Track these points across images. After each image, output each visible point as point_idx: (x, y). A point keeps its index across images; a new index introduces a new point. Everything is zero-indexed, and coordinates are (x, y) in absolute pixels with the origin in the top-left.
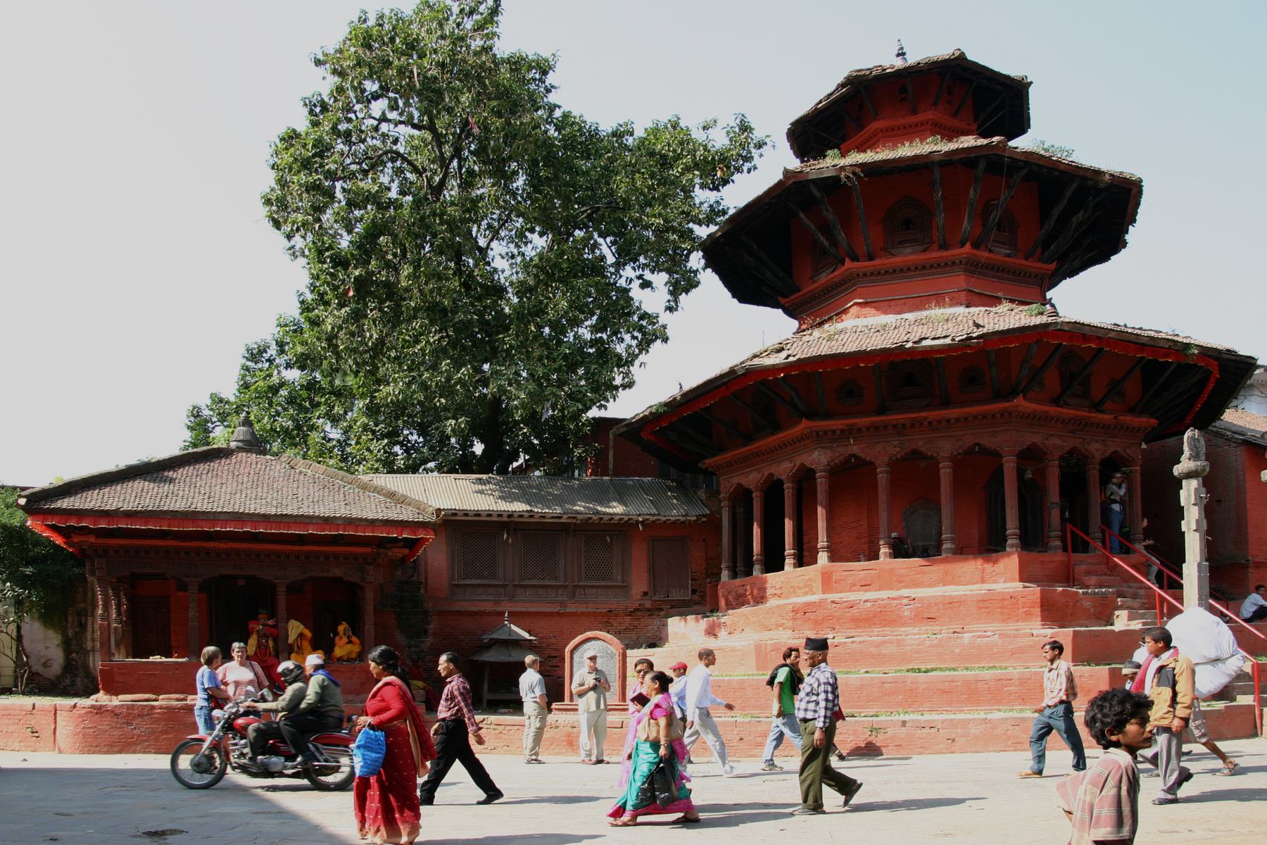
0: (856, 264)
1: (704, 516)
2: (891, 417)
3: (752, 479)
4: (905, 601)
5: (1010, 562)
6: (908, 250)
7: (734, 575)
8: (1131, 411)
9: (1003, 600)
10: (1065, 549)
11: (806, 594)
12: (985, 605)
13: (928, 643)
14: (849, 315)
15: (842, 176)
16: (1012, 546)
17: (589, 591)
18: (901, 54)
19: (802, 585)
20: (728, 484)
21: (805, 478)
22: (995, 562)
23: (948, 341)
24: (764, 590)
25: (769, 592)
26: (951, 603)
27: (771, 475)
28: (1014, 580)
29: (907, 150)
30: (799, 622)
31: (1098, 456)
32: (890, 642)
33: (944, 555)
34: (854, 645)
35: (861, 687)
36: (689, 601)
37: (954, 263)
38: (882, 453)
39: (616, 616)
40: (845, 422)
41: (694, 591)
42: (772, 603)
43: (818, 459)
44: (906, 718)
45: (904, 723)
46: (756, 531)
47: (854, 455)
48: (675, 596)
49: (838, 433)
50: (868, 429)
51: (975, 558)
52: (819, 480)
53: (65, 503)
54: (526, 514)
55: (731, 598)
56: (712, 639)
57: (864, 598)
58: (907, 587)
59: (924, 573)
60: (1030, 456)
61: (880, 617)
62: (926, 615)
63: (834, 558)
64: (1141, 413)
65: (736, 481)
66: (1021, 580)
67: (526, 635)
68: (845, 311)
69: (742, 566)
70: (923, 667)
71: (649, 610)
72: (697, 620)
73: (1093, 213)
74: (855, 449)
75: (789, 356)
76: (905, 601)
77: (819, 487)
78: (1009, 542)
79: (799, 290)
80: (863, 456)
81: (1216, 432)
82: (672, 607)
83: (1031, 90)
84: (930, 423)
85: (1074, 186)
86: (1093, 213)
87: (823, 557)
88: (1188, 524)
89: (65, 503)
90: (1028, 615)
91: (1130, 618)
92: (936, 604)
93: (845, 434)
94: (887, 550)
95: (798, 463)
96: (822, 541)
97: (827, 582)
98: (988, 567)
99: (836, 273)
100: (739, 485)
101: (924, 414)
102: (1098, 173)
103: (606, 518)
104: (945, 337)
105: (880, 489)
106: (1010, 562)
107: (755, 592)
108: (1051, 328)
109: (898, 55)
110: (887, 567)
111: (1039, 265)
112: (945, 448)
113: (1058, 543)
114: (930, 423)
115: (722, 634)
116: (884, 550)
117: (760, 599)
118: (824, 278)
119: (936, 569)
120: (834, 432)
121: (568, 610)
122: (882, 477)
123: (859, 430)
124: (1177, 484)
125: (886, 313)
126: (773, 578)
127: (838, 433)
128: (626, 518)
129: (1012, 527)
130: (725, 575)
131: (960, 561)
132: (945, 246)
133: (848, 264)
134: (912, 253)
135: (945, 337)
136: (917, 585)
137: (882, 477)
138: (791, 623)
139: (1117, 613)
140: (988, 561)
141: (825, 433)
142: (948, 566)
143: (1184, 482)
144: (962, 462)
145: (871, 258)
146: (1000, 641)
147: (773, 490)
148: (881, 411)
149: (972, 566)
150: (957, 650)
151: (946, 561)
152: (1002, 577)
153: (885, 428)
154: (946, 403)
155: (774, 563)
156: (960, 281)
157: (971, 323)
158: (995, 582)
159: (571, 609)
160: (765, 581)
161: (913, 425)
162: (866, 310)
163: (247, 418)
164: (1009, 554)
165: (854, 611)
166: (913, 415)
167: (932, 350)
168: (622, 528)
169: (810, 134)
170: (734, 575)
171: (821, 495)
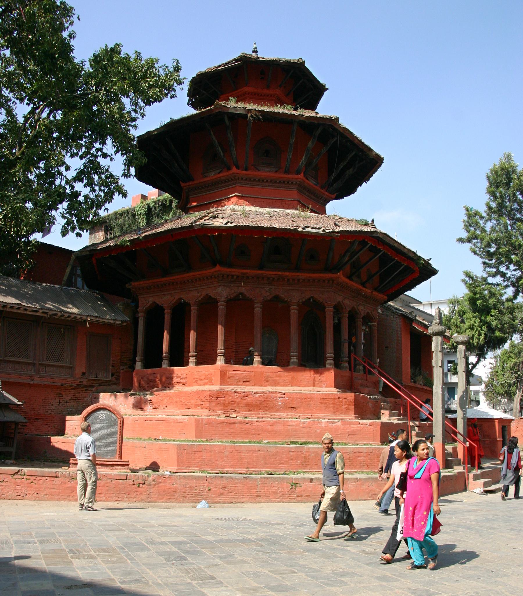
0: (238, 171)
1: (125, 321)
2: (267, 272)
3: (166, 300)
4: (279, 395)
5: (330, 375)
6: (267, 169)
7: (146, 365)
9: (335, 399)
10: (350, 370)
11: (205, 384)
12: (325, 401)
13: (302, 425)
14: (230, 202)
15: (249, 114)
16: (330, 364)
17: (48, 369)
18: (255, 51)
19: (202, 378)
20: (146, 301)
21: (208, 306)
22: (321, 373)
23: (320, 231)
24: (171, 378)
25: (175, 380)
26: (305, 399)
27: (181, 299)
28: (330, 387)
29: (278, 109)
30: (214, 404)
31: (363, 314)
32: (279, 423)
33: (291, 366)
34: (258, 423)
35: (276, 454)
36: (110, 381)
38: (258, 294)
39: (66, 389)
40: (241, 271)
41: (113, 375)
42: (177, 389)
43: (222, 293)
44: (313, 476)
45: (311, 480)
46: (166, 336)
47: (242, 294)
48: (102, 377)
49: (235, 277)
50: (253, 277)
51: (310, 370)
54: (16, 306)
55: (143, 382)
56: (139, 412)
57: (255, 391)
58: (270, 385)
59: (281, 376)
60: (338, 309)
61: (263, 405)
62: (291, 406)
63: (227, 362)
65: (151, 300)
66: (335, 387)
67: (15, 401)
68: (229, 199)
69: (153, 360)
70: (300, 441)
71: (85, 386)
72: (126, 397)
74: (243, 290)
75: (228, 222)
76: (279, 395)
79: (193, 180)
80: (248, 295)
81: (387, 307)
82: (100, 385)
83: (326, 93)
84: (288, 280)
85: (353, 154)
86: (350, 164)
87: (220, 361)
88: (437, 362)
90: (348, 409)
91: (390, 416)
92: (297, 399)
94: (259, 359)
95: (204, 294)
96: (220, 349)
97: (224, 378)
98: (317, 376)
99: (221, 175)
100: (154, 302)
101: (287, 273)
102: (370, 150)
103: (66, 315)
104: (319, 228)
105: (292, 322)
106: (330, 375)
107: (164, 379)
108: (374, 235)
109: (254, 52)
110: (260, 370)
112: (295, 297)
113: (347, 365)
114: (288, 280)
115: (148, 408)
116: (257, 359)
117: (168, 384)
118: (212, 175)
119: (288, 375)
120: (233, 276)
121: (36, 382)
123: (248, 278)
124: (429, 339)
125: (252, 205)
126: (178, 370)
127: (235, 277)
128: (79, 317)
129: (330, 353)
130: (138, 365)
131: (301, 371)
132: (287, 172)
133: (234, 170)
134: (270, 171)
135: (319, 228)
136: (276, 384)
138: (208, 405)
139: (382, 411)
140: (316, 372)
141: (228, 276)
142: (295, 374)
143: (434, 338)
144: (267, 305)
145: (246, 170)
146: (342, 426)
147: (180, 311)
148: (261, 268)
149: (308, 375)
150: (318, 431)
151: (293, 370)
152: (321, 385)
154: (298, 269)
155: (179, 359)
156: (294, 194)
157: (333, 223)
158: (321, 387)
159: (37, 381)
160: (173, 372)
162: (242, 201)
164: (329, 370)
165: (248, 399)
166: (280, 273)
167: (311, 235)
168: (73, 324)
170: (146, 365)
171: (221, 317)
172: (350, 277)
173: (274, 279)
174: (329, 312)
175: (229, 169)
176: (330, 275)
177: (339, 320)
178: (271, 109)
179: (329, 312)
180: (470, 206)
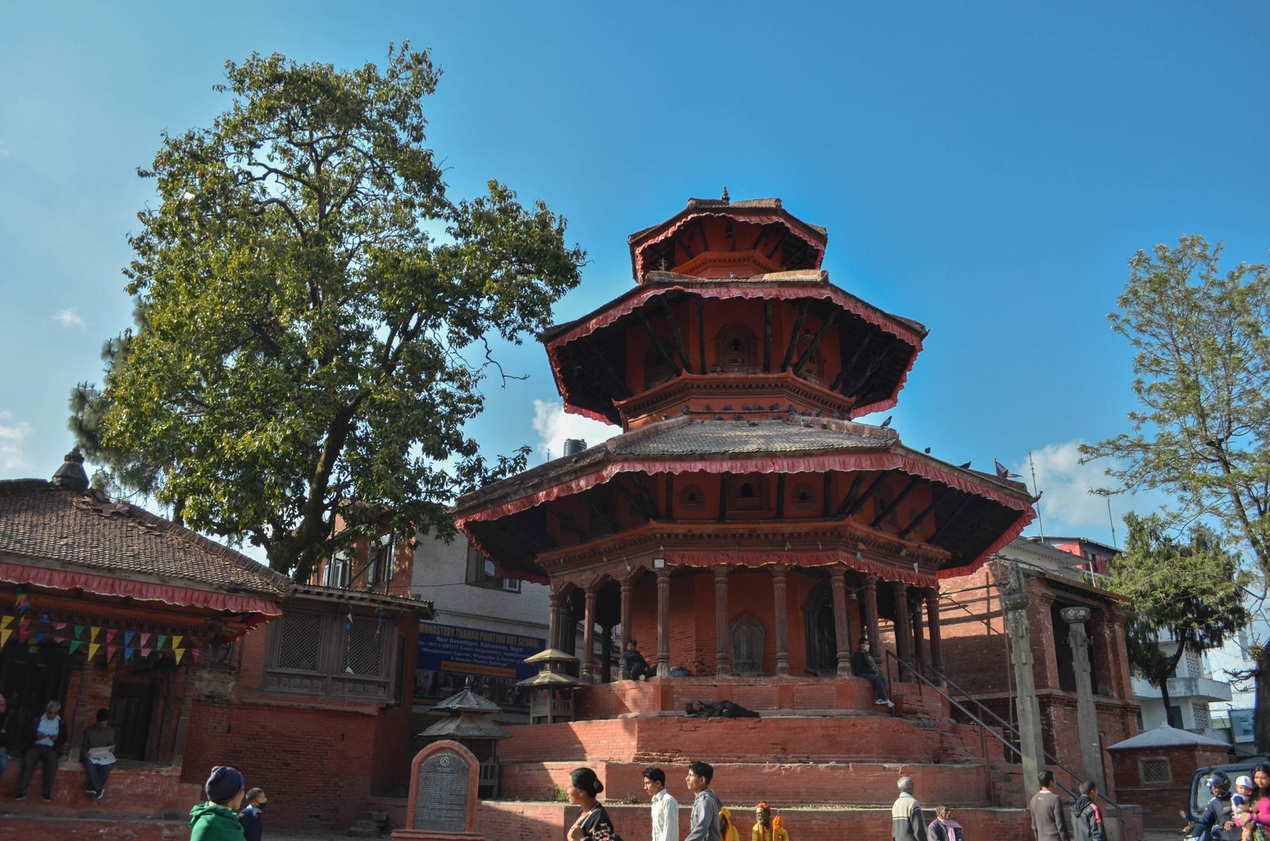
2: (732, 526)
3: (585, 578)
8: (929, 541)
16: (843, 669)
27: (607, 576)
37: (776, 385)
49: (681, 537)
52: (661, 585)
53: (1057, 546)
64: (937, 544)
65: (567, 579)
73: (871, 356)
77: (660, 592)
78: (841, 665)
79: (632, 395)
86: (871, 356)
89: (1057, 546)
93: (691, 540)
95: (638, 565)
99: (670, 382)
100: (571, 583)
111: (841, 396)
120: (677, 535)
122: (721, 588)
127: (681, 537)
137: (721, 588)
153: (725, 536)
154: (779, 516)
161: (750, 535)
163: (393, 116)
169: (656, 252)
172: (874, 524)
173: (742, 535)
174: (838, 584)
175: (679, 374)
176: (831, 524)
177: (861, 595)
178: (829, 809)
179: (838, 584)
180: (1132, 369)
